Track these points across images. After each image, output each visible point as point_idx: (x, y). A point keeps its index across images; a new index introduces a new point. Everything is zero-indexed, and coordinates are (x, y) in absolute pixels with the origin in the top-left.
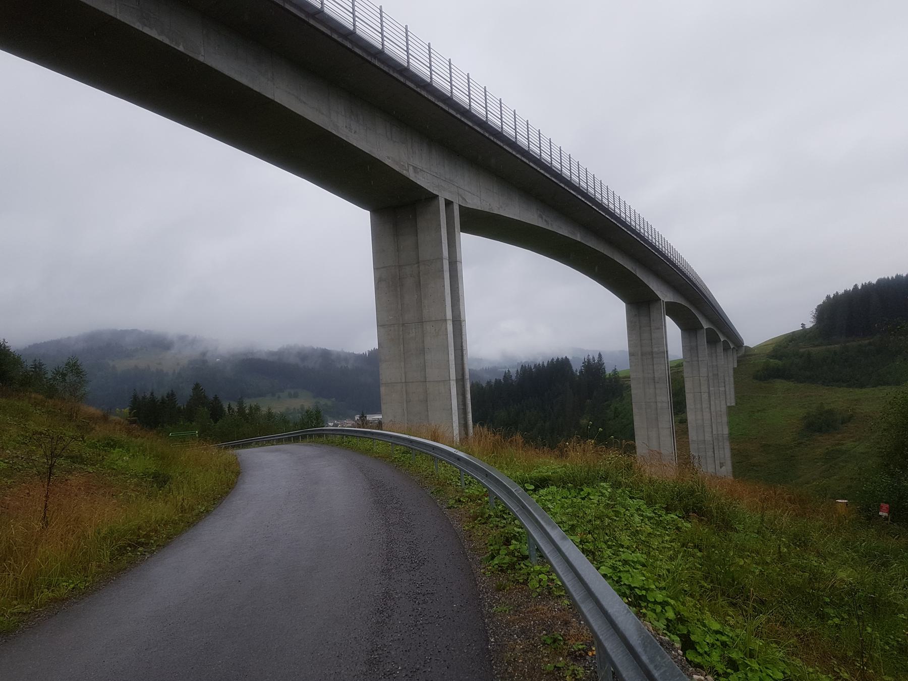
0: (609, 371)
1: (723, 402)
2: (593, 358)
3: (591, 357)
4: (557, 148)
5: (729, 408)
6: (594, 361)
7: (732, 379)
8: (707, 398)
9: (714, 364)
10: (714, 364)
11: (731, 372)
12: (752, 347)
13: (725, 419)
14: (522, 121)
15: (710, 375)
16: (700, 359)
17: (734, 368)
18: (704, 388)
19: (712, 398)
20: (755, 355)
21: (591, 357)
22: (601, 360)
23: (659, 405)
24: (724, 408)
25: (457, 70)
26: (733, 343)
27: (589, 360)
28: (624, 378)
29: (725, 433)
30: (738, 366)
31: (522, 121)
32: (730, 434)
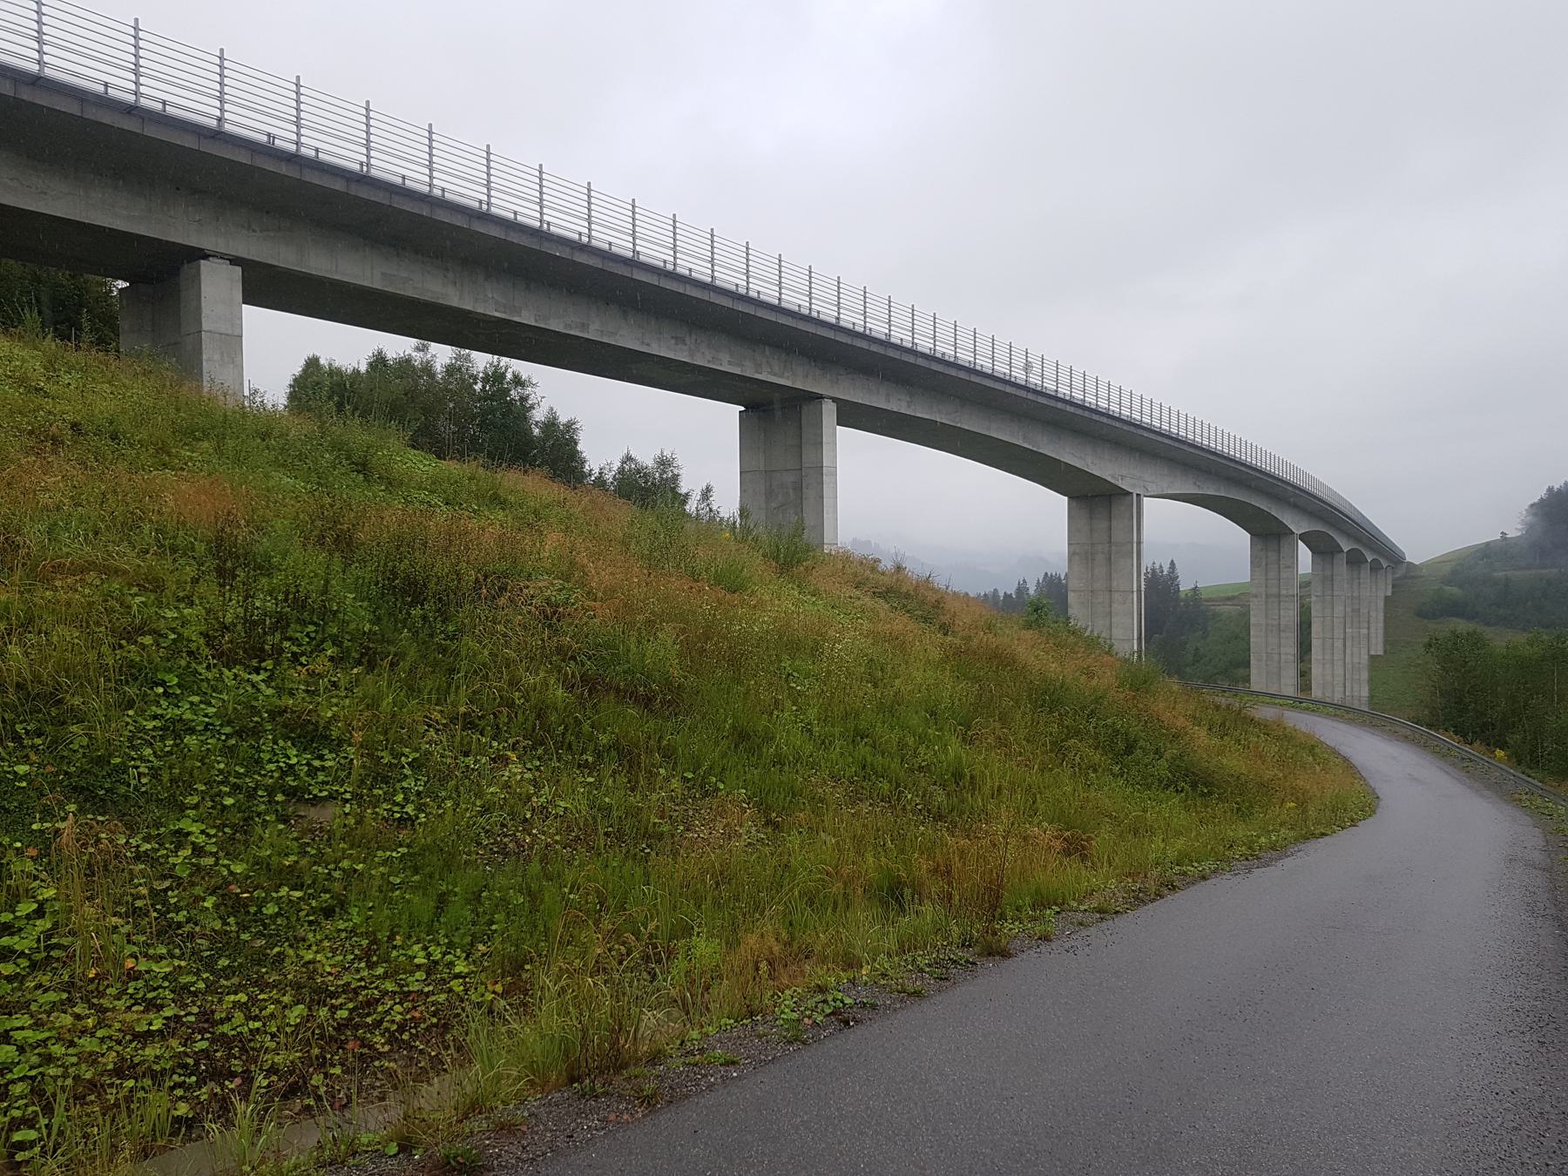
0: (1185, 586)
1: (1364, 651)
2: (1161, 567)
3: (1157, 566)
4: (802, 271)
5: (1373, 659)
6: (1162, 572)
7: (1381, 616)
8: (1341, 646)
9: (1356, 594)
10: (1356, 594)
11: (1381, 604)
12: (1417, 563)
13: (1365, 675)
14: (737, 247)
15: (1348, 609)
16: (1335, 593)
17: (1386, 597)
18: (1338, 633)
19: (1348, 644)
20: (1421, 577)
21: (1157, 566)
22: (1173, 572)
23: (1283, 657)
24: (1365, 659)
25: (760, 255)
26: (1386, 558)
27: (1153, 570)
28: (1207, 601)
29: (1363, 694)
30: (1393, 593)
31: (737, 247)
32: (1371, 697)
